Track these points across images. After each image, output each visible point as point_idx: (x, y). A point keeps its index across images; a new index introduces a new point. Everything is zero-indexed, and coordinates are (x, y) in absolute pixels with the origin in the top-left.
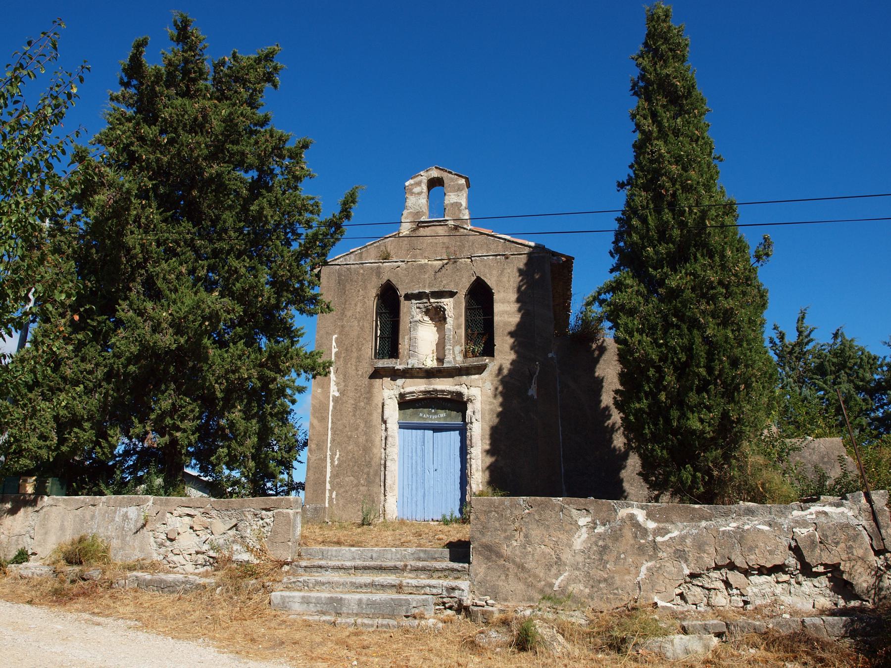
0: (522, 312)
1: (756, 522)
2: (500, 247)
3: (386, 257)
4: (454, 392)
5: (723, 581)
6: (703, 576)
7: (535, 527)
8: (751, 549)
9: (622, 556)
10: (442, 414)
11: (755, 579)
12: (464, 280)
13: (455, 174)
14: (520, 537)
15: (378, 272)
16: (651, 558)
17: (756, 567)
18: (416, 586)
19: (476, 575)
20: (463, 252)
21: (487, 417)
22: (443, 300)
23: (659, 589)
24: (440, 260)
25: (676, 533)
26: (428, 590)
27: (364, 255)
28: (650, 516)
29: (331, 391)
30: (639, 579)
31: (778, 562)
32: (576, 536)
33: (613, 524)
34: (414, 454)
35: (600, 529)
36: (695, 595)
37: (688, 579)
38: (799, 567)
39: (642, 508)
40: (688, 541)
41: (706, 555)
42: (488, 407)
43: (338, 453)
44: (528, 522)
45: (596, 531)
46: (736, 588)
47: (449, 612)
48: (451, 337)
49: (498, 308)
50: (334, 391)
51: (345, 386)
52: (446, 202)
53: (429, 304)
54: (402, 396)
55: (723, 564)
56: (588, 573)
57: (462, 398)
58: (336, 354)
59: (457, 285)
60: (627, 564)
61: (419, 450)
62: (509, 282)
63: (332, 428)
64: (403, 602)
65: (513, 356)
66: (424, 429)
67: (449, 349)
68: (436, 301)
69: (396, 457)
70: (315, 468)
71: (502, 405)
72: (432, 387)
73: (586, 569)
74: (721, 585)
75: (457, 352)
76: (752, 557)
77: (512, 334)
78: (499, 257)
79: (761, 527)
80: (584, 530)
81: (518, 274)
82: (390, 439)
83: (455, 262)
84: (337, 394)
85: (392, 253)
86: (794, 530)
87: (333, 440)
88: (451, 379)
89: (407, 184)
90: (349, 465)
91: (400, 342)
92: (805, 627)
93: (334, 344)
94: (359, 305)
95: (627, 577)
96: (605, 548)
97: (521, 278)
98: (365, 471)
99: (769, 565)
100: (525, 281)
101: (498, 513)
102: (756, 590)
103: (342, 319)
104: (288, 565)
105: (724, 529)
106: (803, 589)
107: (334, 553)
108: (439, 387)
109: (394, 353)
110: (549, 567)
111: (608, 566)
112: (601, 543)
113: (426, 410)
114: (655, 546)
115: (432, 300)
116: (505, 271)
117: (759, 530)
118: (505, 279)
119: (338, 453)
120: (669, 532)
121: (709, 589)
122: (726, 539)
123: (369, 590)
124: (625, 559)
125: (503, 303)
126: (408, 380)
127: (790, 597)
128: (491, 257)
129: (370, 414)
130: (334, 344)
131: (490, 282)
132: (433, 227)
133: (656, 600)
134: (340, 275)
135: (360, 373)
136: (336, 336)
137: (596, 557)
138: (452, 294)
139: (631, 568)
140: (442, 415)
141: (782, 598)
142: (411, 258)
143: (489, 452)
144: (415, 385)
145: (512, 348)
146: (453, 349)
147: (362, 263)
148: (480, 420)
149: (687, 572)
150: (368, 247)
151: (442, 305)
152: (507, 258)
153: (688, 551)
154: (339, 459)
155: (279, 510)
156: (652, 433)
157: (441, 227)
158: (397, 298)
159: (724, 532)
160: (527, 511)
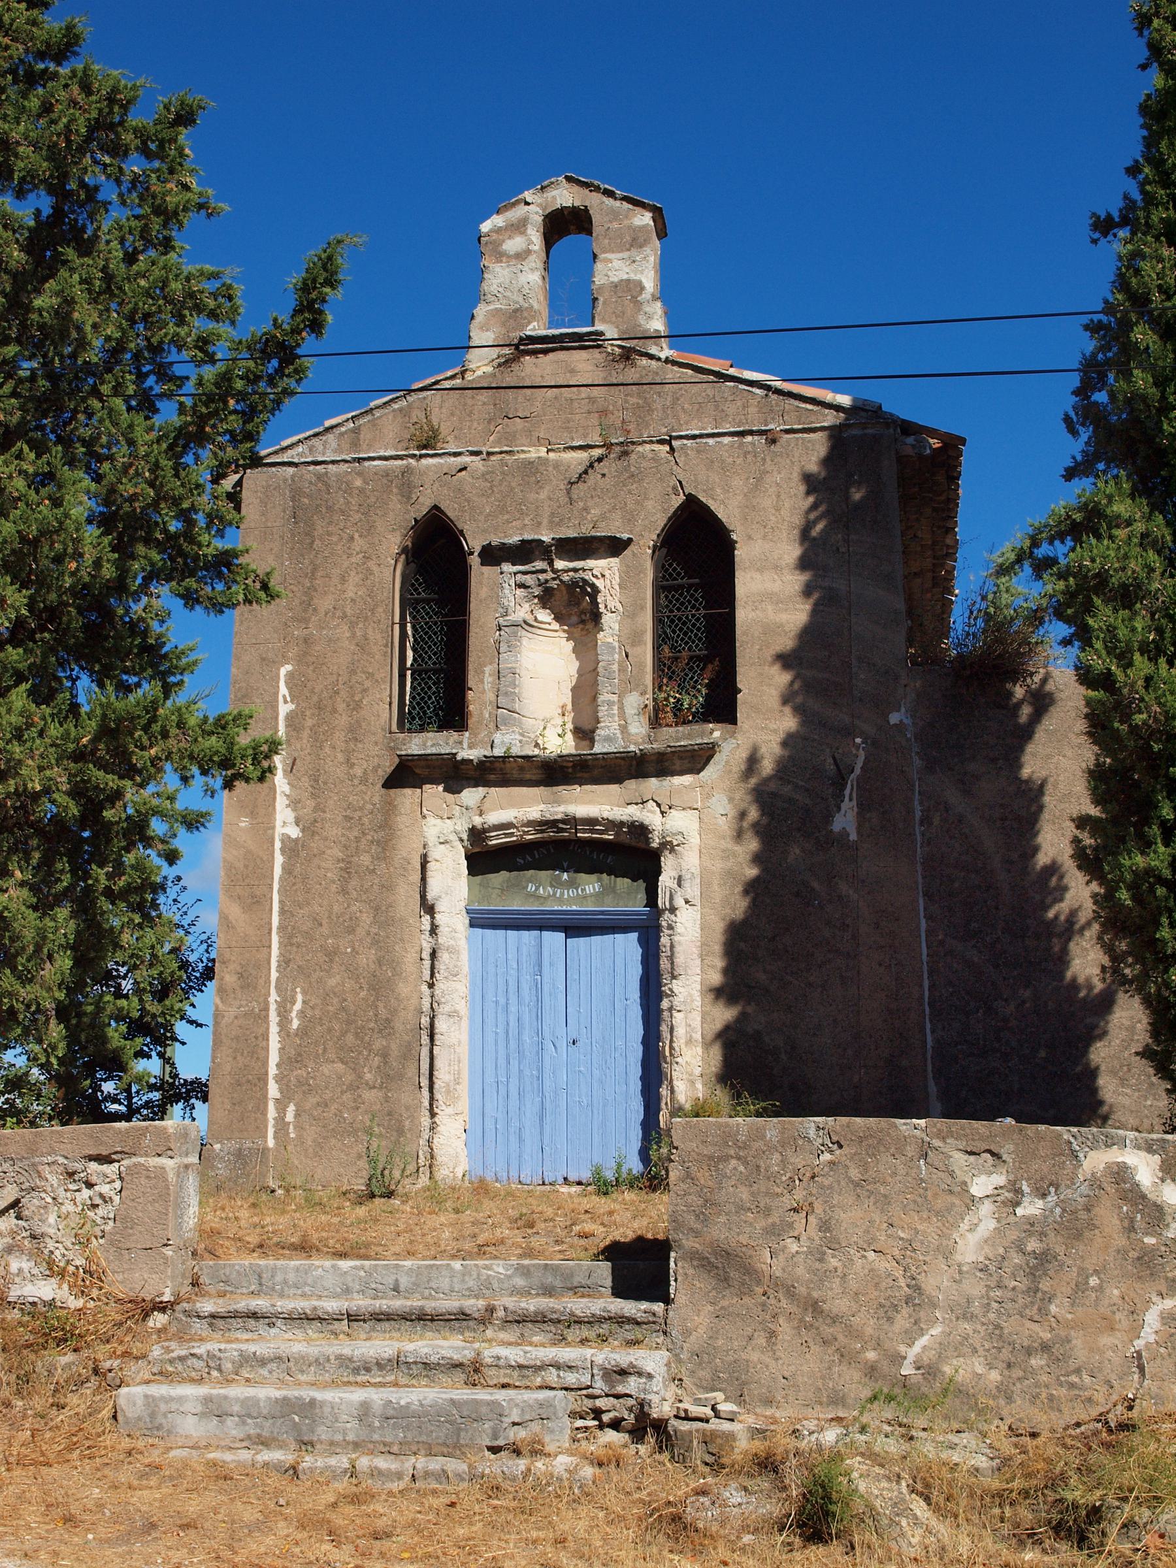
0: (816, 596)
3: (428, 443)
4: (622, 824)
7: (851, 1200)
9: (1093, 1281)
10: (591, 885)
12: (649, 504)
13: (625, 199)
15: (406, 484)
19: (687, 1333)
20: (647, 426)
22: (590, 563)
24: (581, 448)
26: (552, 1376)
27: (365, 435)
29: (278, 823)
30: (1139, 1344)
32: (964, 1226)
35: (1031, 1208)
42: (718, 866)
43: (299, 998)
44: (830, 1187)
45: (1020, 1211)
47: (611, 1436)
48: (615, 667)
49: (746, 584)
50: (285, 824)
51: (317, 809)
52: (599, 280)
53: (550, 575)
54: (477, 835)
56: (998, 1327)
57: (647, 840)
58: (290, 718)
59: (630, 519)
62: (778, 510)
63: (282, 928)
65: (788, 722)
67: (610, 704)
68: (571, 565)
69: (462, 1007)
70: (237, 1038)
72: (562, 809)
73: (992, 1316)
75: (630, 711)
77: (785, 660)
78: (749, 438)
83: (626, 453)
84: (294, 832)
85: (444, 430)
87: (285, 962)
88: (614, 788)
89: (485, 227)
90: (330, 1030)
91: (471, 684)
93: (283, 690)
94: (354, 579)
95: (1106, 1340)
96: (1044, 1258)
97: (811, 499)
100: (821, 509)
101: (746, 1163)
103: (306, 621)
104: (163, 1310)
107: (291, 1277)
108: (581, 810)
110: (887, 1311)
111: (1053, 1308)
112: (1033, 1245)
113: (544, 875)
115: (560, 564)
116: (768, 479)
118: (767, 502)
119: (299, 998)
124: (1100, 1289)
125: (760, 570)
126: (493, 789)
129: (388, 887)
130: (283, 690)
131: (726, 510)
135: (358, 771)
136: (289, 667)
137: (1022, 1284)
138: (615, 546)
139: (1118, 1316)
142: (498, 442)
146: (620, 702)
147: (359, 460)
148: (697, 901)
150: (377, 414)
151: (588, 576)
152: (774, 441)
157: (583, 354)
160: (827, 1157)
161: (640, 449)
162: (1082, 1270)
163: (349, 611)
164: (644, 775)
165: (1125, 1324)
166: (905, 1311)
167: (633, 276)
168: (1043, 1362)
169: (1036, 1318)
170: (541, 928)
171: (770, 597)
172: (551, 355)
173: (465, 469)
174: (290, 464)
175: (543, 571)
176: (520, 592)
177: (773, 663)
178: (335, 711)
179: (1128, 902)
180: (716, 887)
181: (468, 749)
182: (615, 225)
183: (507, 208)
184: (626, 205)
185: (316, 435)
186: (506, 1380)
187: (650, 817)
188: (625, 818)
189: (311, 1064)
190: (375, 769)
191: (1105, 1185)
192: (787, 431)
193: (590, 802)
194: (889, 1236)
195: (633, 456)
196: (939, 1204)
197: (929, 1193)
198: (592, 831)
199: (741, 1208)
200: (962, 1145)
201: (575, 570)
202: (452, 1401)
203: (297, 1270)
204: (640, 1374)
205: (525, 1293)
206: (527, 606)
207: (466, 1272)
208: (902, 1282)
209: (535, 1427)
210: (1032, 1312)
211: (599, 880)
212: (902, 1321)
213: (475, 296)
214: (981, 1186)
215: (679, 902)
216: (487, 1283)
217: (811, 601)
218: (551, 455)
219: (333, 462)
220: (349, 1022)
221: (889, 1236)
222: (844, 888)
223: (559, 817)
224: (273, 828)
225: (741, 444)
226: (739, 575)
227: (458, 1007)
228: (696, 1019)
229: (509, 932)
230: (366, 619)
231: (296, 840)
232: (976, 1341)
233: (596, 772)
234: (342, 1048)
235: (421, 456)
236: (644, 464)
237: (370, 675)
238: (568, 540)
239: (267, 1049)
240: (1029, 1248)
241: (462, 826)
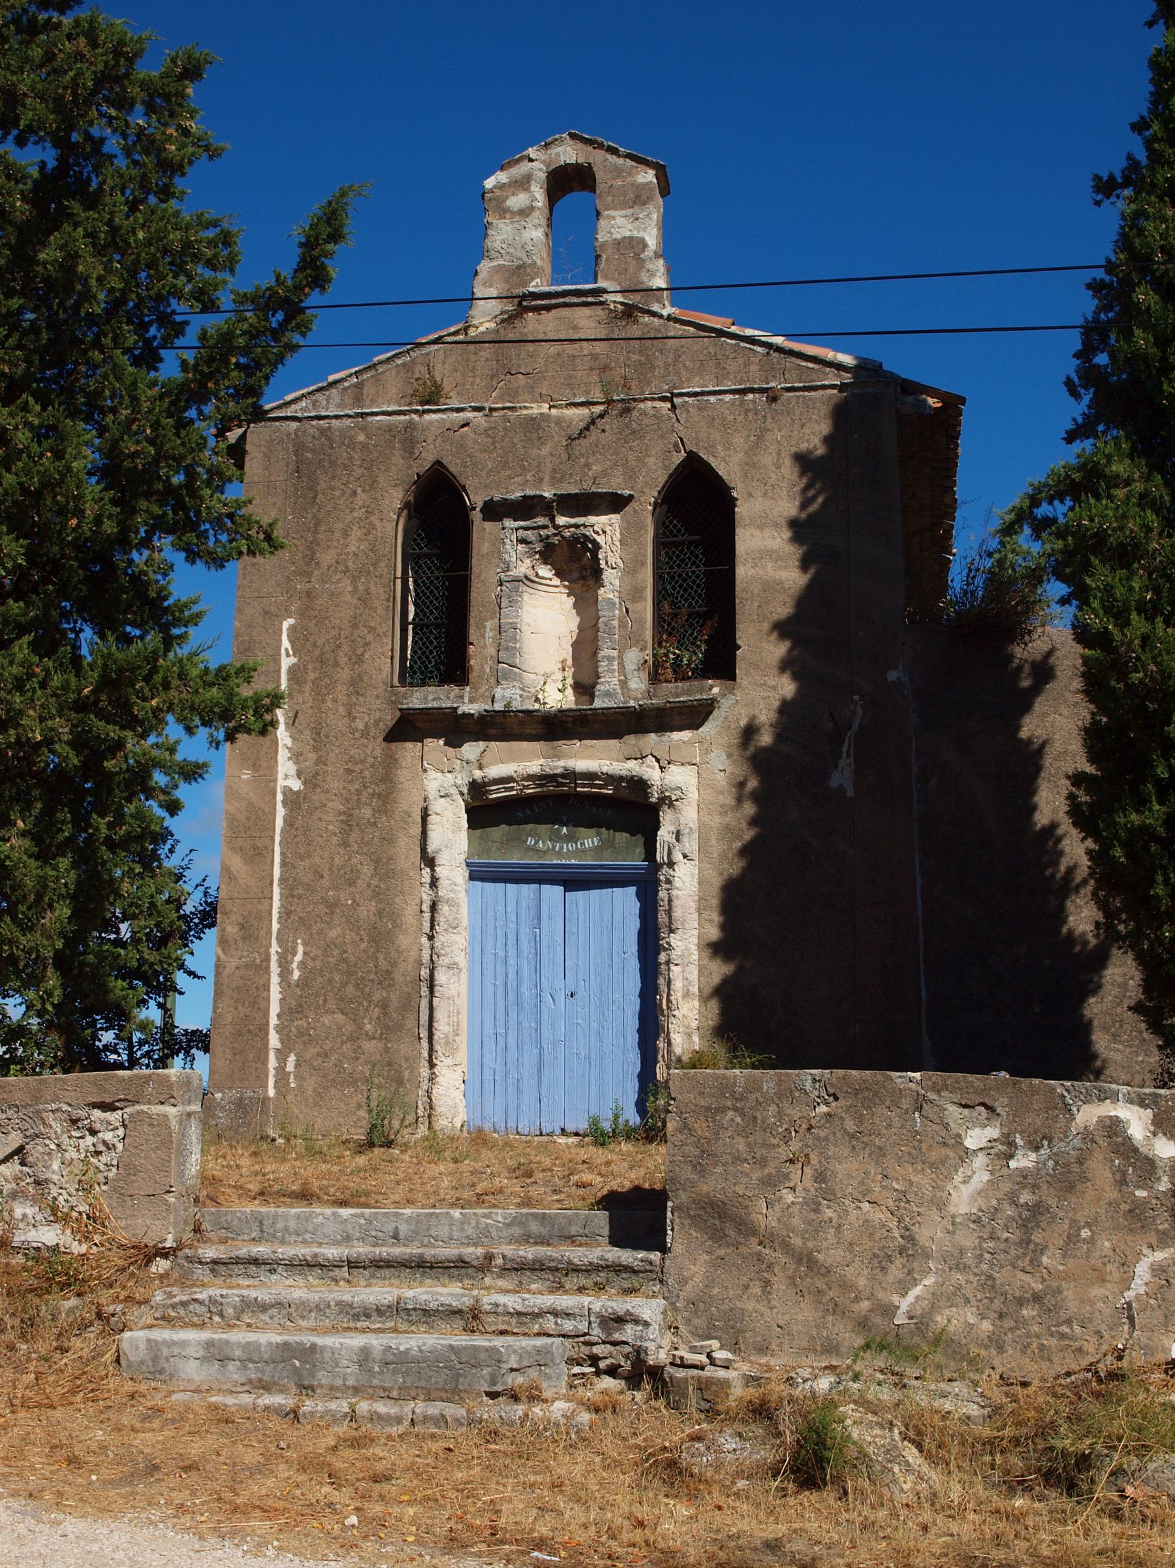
3: (431, 397)
7: (846, 1152)
9: (1085, 1233)
10: (590, 840)
12: (651, 461)
13: (628, 156)
14: (803, 1180)
15: (409, 438)
18: (519, 1314)
19: (683, 1281)
20: (649, 383)
22: (592, 519)
24: (582, 404)
26: (550, 1323)
27: (369, 390)
29: (280, 776)
30: (1129, 1295)
32: (958, 1178)
34: (512, 952)
35: (1024, 1160)
39: (1142, 1104)
42: (716, 821)
43: (300, 949)
44: (826, 1139)
45: (1013, 1164)
48: (616, 623)
49: (747, 541)
50: (287, 776)
51: (317, 763)
52: (602, 237)
53: (552, 531)
54: (477, 788)
56: (990, 1277)
57: (647, 795)
58: (292, 671)
59: (631, 475)
60: (1097, 1254)
62: (778, 468)
63: (283, 880)
67: (610, 659)
68: (573, 521)
69: (461, 959)
70: (238, 988)
72: (561, 763)
73: (984, 1267)
75: (630, 666)
78: (750, 396)
83: (627, 410)
84: (296, 785)
85: (447, 386)
87: (286, 914)
88: (613, 743)
89: (489, 183)
90: (330, 981)
91: (472, 638)
93: (286, 643)
94: (356, 533)
95: (1096, 1291)
96: (1037, 1211)
103: (309, 575)
107: (292, 1224)
111: (1045, 1260)
112: (1025, 1197)
113: (543, 828)
115: (561, 520)
116: (769, 437)
118: (768, 460)
119: (300, 949)
124: (1092, 1241)
125: (761, 527)
128: (728, 398)
130: (286, 643)
131: (727, 467)
134: (299, 449)
135: (360, 725)
136: (291, 621)
137: (1014, 1235)
138: (615, 503)
139: (1109, 1267)
140: (588, 843)
142: (501, 398)
146: (620, 657)
148: (695, 856)
151: (589, 532)
152: (774, 399)
154: (302, 964)
155: (138, 1107)
160: (823, 1109)
161: (641, 405)
162: (1074, 1222)
163: (351, 565)
165: (1116, 1276)
166: (899, 1262)
167: (635, 234)
169: (1028, 1269)
172: (554, 312)
175: (545, 527)
176: (521, 548)
178: (337, 664)
180: (714, 842)
182: (619, 183)
183: (511, 164)
184: (629, 163)
186: (504, 1327)
187: (650, 772)
188: (623, 773)
189: (312, 1015)
190: (376, 723)
191: (1097, 1138)
192: (788, 390)
193: (590, 757)
194: (884, 1187)
195: (635, 413)
196: (934, 1156)
201: (577, 526)
203: (298, 1217)
204: (636, 1321)
206: (528, 562)
207: (465, 1220)
211: (598, 834)
212: (896, 1271)
213: (482, 253)
214: (975, 1138)
218: (554, 411)
219: (337, 417)
221: (884, 1187)
223: (559, 771)
224: (276, 780)
225: (742, 402)
226: (737, 531)
227: (457, 960)
228: (693, 973)
229: (545, 887)
232: (968, 1291)
234: (342, 999)
235: (425, 412)
237: (372, 629)
239: (268, 1000)
240: (1022, 1201)
241: (463, 780)
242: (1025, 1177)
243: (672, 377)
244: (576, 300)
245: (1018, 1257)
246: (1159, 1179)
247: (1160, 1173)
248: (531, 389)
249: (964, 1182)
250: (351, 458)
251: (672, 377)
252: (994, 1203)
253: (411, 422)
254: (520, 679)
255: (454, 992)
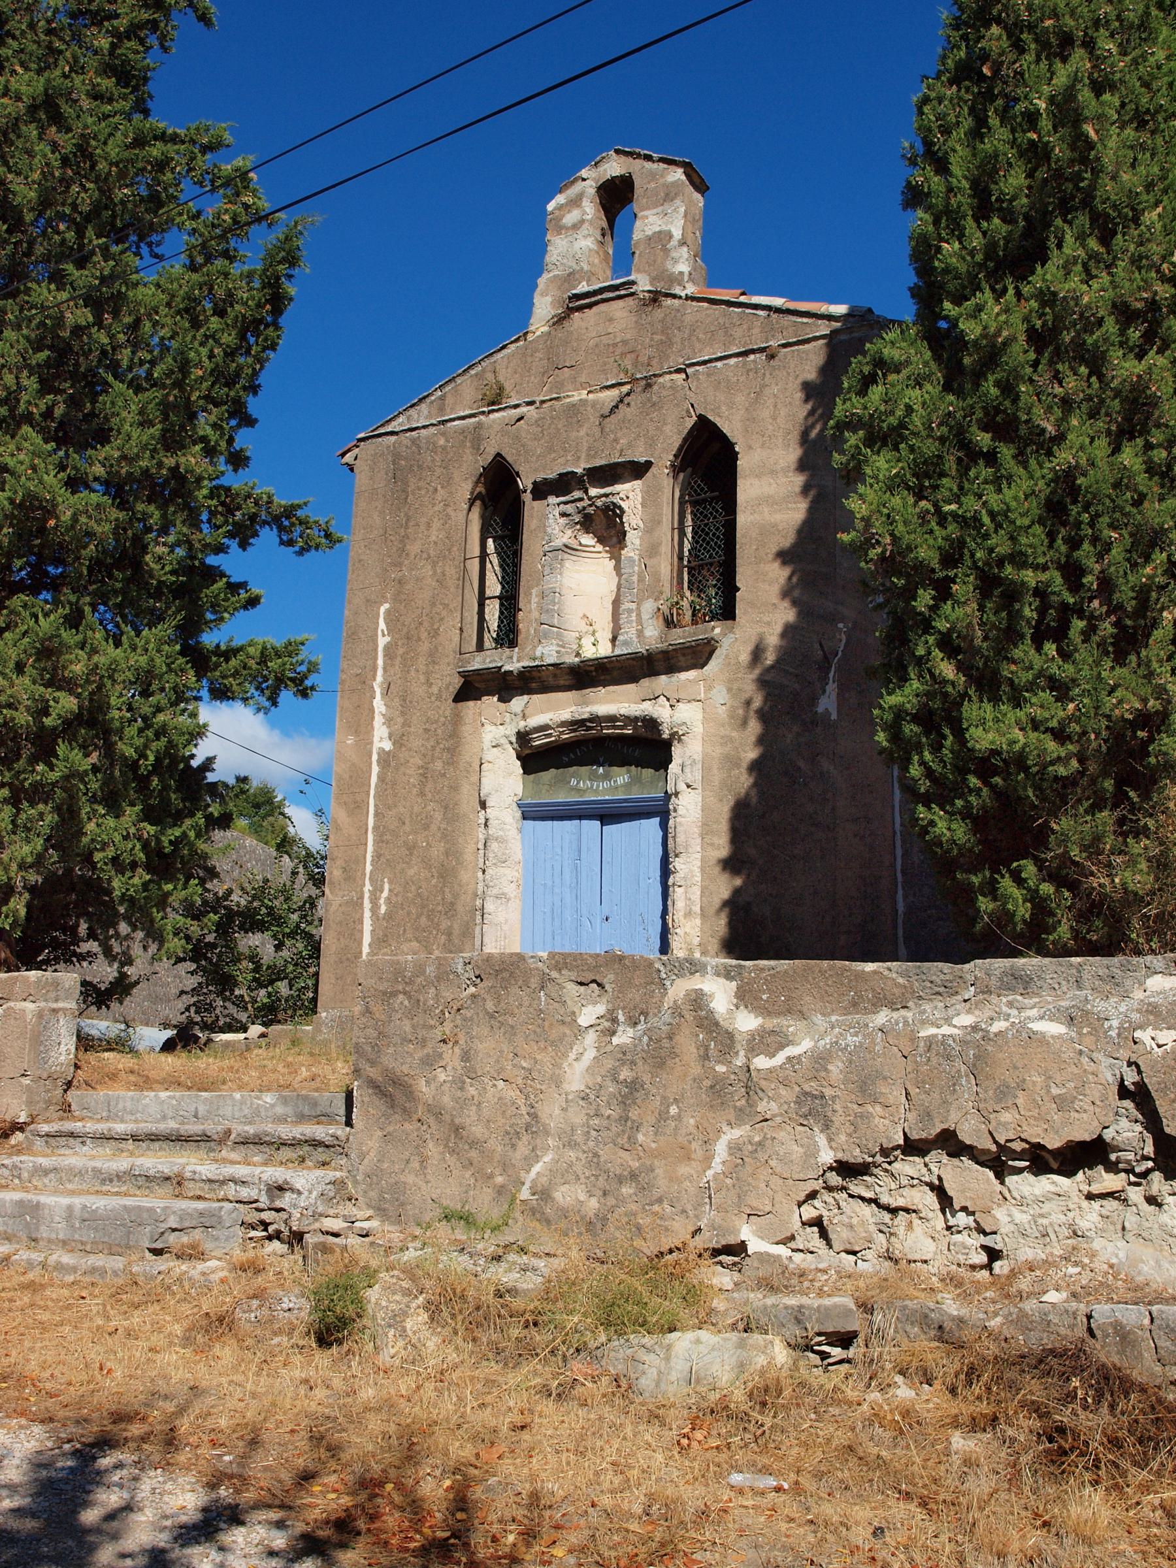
0: (813, 493)
1: (1034, 1013)
2: (756, 331)
3: (495, 400)
4: (636, 719)
5: (931, 1186)
6: (876, 1171)
7: (485, 1031)
8: (1004, 1093)
9: (673, 1110)
10: (621, 776)
11: (1025, 1184)
12: (667, 429)
13: (661, 160)
14: (451, 1056)
15: (476, 437)
16: (741, 1116)
17: (1018, 1146)
18: (210, 1181)
19: (362, 1156)
20: (668, 358)
21: (717, 777)
22: (618, 488)
23: (755, 1204)
24: (613, 386)
25: (804, 1046)
26: (231, 1190)
27: (449, 400)
28: (745, 997)
29: (376, 739)
30: (710, 1173)
31: (1084, 1134)
32: (572, 1056)
33: (654, 1021)
34: (557, 881)
35: (624, 1036)
36: (851, 1226)
37: (834, 1179)
38: (1149, 1150)
39: (728, 976)
40: (836, 1069)
41: (878, 1108)
42: (718, 751)
43: (387, 887)
44: (471, 1019)
45: (616, 1040)
46: (964, 1209)
47: (276, 1244)
48: (635, 578)
49: (747, 490)
50: (381, 739)
51: (404, 725)
52: (637, 236)
53: (587, 502)
54: (523, 737)
55: (924, 1135)
56: (596, 1155)
57: (659, 733)
58: (387, 648)
59: (651, 444)
60: (683, 1131)
61: (567, 870)
62: (775, 419)
63: (375, 828)
64: (145, 1215)
65: (786, 614)
66: (580, 818)
67: (630, 611)
68: (602, 491)
69: (511, 890)
70: (340, 923)
71: (761, 741)
72: (588, 709)
73: (591, 1144)
74: (928, 1200)
75: (645, 616)
76: (1006, 1117)
77: (784, 556)
78: (752, 357)
79: (1037, 1026)
80: (591, 1037)
81: (799, 396)
82: (494, 846)
83: (649, 386)
84: (387, 746)
85: (508, 386)
86: (1138, 1034)
87: (377, 856)
88: (631, 688)
89: (550, 207)
90: (409, 913)
91: (521, 605)
92: (1090, 1331)
93: (382, 625)
94: (436, 524)
95: (684, 1170)
96: (634, 1086)
97: (809, 406)
98: (443, 926)
99: (1053, 1142)
100: (820, 411)
101: (410, 998)
102: (1021, 1217)
103: (400, 564)
104: (22, 1130)
105: (933, 1031)
106: (1164, 1218)
107: (129, 1105)
108: (603, 709)
109: (509, 636)
110: (512, 1138)
111: (640, 1137)
112: (625, 1074)
113: (584, 770)
114: (750, 1083)
115: (593, 492)
116: (767, 391)
117: (1032, 1036)
118: (766, 413)
119: (387, 887)
120: (789, 1043)
121: (893, 1211)
122: (934, 1061)
123: (124, 1189)
124: (678, 1118)
125: (758, 476)
126: (535, 697)
127: (1121, 1244)
128: (733, 361)
129: (455, 788)
130: (382, 625)
131: (730, 426)
132: (603, 307)
133: (746, 1233)
134: (397, 457)
135: (435, 690)
136: (387, 606)
137: (614, 1112)
138: (638, 470)
139: (694, 1145)
140: (620, 781)
141: (1097, 1244)
142: (550, 391)
143: (730, 865)
144: (549, 710)
145: (786, 594)
146: (638, 609)
147: (444, 422)
148: (698, 785)
149: (827, 1157)
150: (459, 381)
151: (616, 500)
152: (772, 357)
153: (834, 1098)
154: (388, 899)
155: (11, 1004)
156: (929, 773)
157: (620, 303)
158: (518, 493)
159: (930, 1042)
160: (472, 989)
161: (661, 380)
162: (664, 1098)
163: (432, 553)
164: (654, 673)
165: (699, 1154)
166: (525, 1138)
167: (664, 228)
168: (631, 1191)
169: (626, 1146)
170: (580, 818)
171: (767, 500)
172: (595, 309)
173: (519, 420)
174: (392, 433)
175: (581, 499)
176: (563, 521)
177: (775, 559)
178: (419, 639)
179: (885, 743)
180: (715, 771)
181: (513, 662)
182: (653, 185)
183: (567, 187)
184: (662, 166)
185: (412, 406)
186: (199, 1193)
187: (661, 712)
188: (637, 714)
189: (394, 944)
190: (447, 688)
191: (684, 1013)
192: (784, 346)
193: (612, 701)
194: (514, 1066)
195: (655, 387)
196: (554, 1034)
197: (546, 1024)
198: (615, 727)
199: (406, 1040)
200: (573, 975)
201: (606, 495)
202: (125, 1207)
203: (132, 1099)
204: (292, 1190)
205: (282, 1120)
206: (569, 532)
207: (243, 1102)
208: (524, 1110)
209: (197, 1234)
210: (624, 1140)
211: (629, 772)
212: (523, 1149)
213: (538, 267)
214: (589, 1015)
215: (682, 787)
216: (257, 1112)
217: (810, 498)
218: (591, 396)
219: (424, 427)
220: (423, 907)
221: (514, 1066)
222: (826, 765)
223: (586, 716)
224: (372, 743)
225: (745, 364)
226: (740, 483)
227: (506, 890)
228: (696, 893)
229: (584, 822)
230: (445, 557)
231: (388, 753)
232: (578, 1168)
233: (615, 673)
234: (417, 929)
235: (490, 412)
236: (665, 393)
237: (446, 606)
238: (595, 468)
239: (361, 932)
240: (622, 1077)
241: (511, 730)
242: (624, 1054)
243: (688, 351)
244: (611, 295)
245: (618, 1135)
246: (737, 1053)
247: (738, 1047)
248: (574, 379)
249: (576, 1059)
250: (433, 460)
251: (688, 351)
252: (599, 1079)
253: (480, 424)
254: (559, 637)
255: (502, 920)
